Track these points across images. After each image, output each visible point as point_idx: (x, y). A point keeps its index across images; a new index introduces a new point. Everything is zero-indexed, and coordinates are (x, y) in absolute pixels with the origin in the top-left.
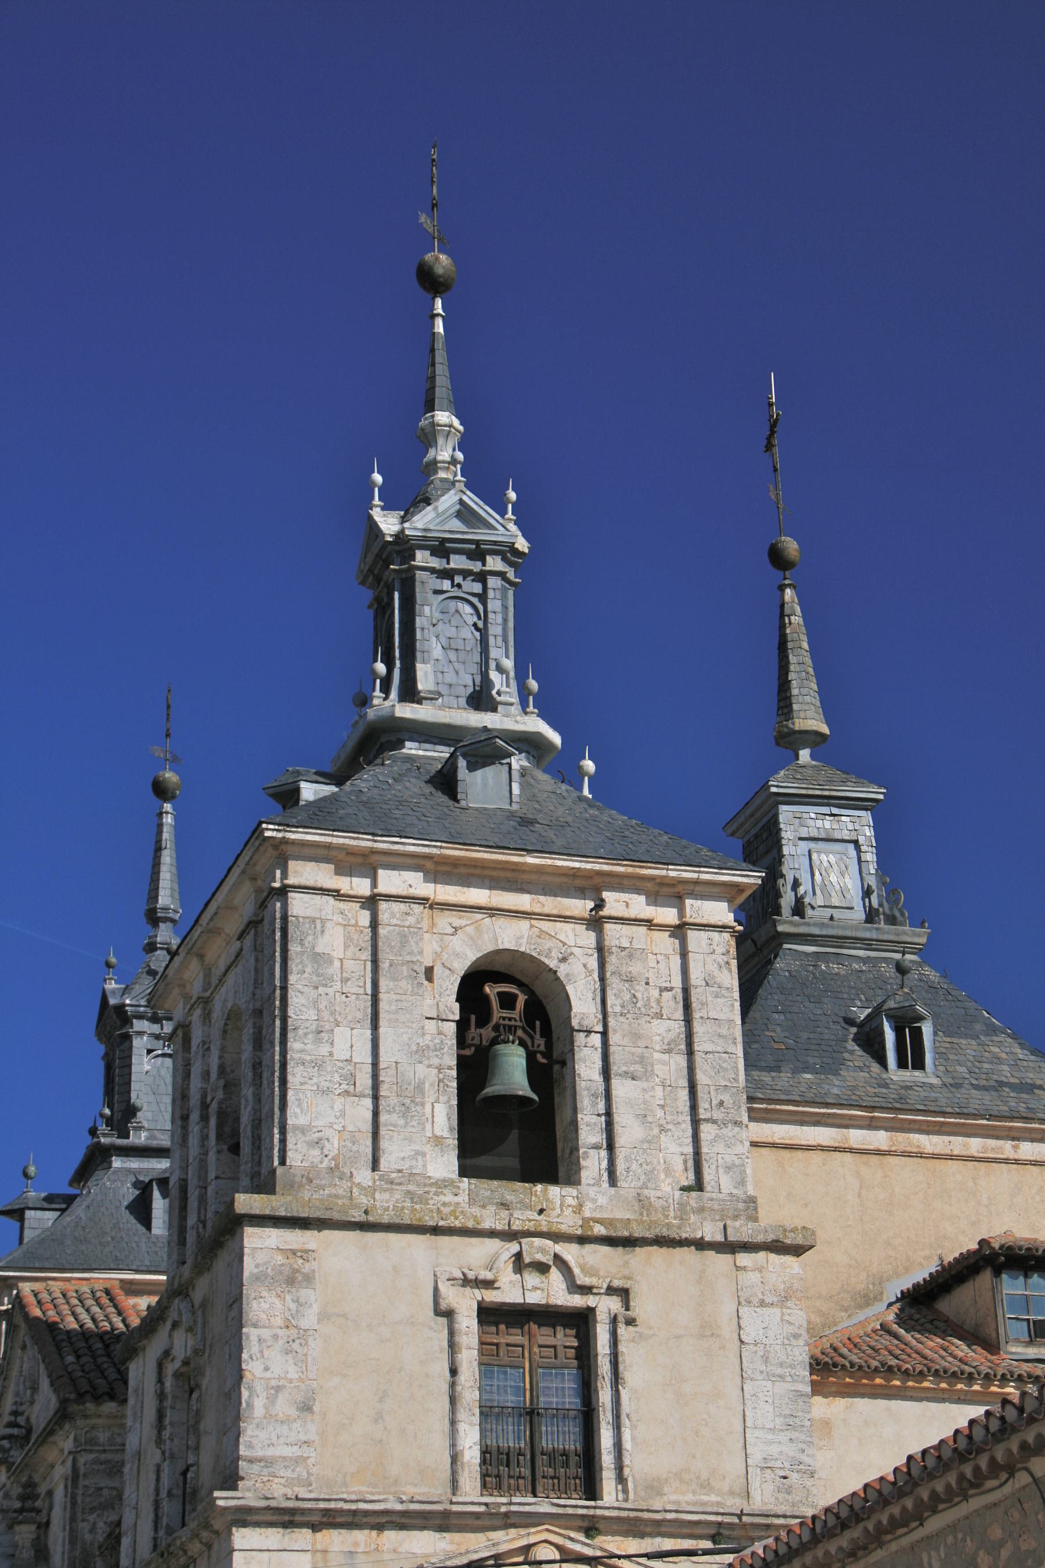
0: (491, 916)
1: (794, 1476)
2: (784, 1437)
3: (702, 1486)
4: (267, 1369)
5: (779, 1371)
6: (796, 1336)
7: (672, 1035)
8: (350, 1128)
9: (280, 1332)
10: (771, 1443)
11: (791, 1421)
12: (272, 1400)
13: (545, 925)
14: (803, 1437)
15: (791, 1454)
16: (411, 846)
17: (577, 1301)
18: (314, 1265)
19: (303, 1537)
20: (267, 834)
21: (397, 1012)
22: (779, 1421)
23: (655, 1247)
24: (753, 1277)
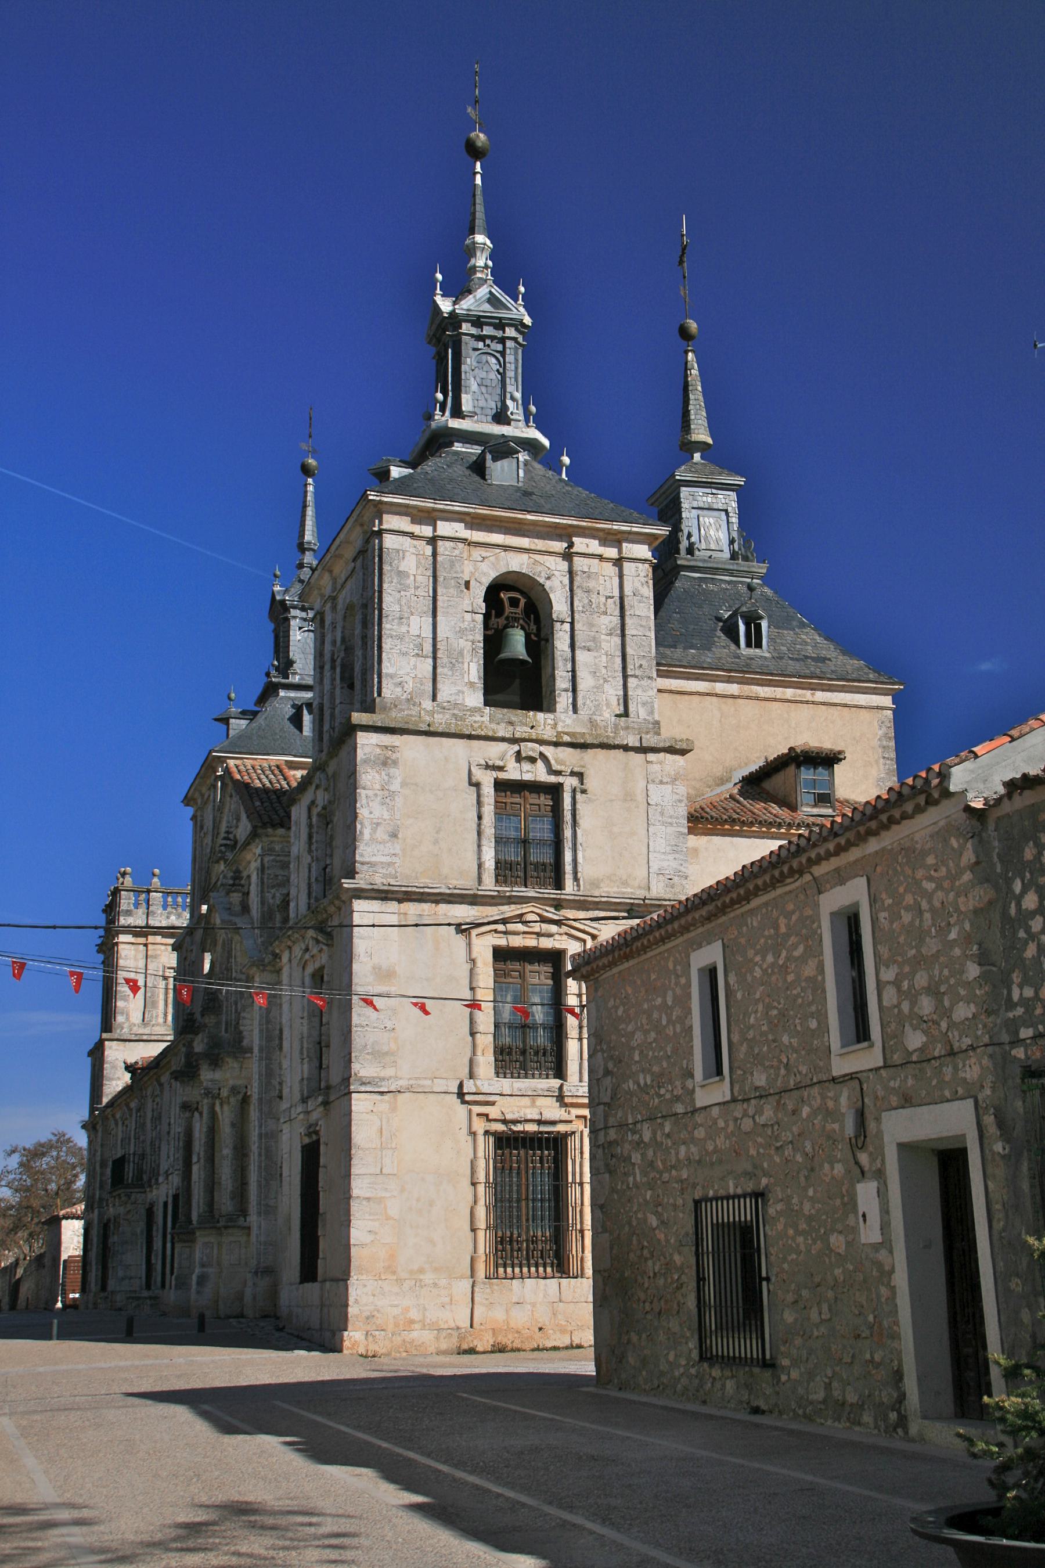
0: (505, 551)
2: (671, 857)
5: (670, 820)
7: (612, 625)
10: (664, 860)
11: (675, 848)
12: (374, 830)
13: (538, 557)
16: (457, 507)
17: (553, 779)
18: (398, 755)
21: (448, 607)
22: (668, 848)
24: (656, 767)
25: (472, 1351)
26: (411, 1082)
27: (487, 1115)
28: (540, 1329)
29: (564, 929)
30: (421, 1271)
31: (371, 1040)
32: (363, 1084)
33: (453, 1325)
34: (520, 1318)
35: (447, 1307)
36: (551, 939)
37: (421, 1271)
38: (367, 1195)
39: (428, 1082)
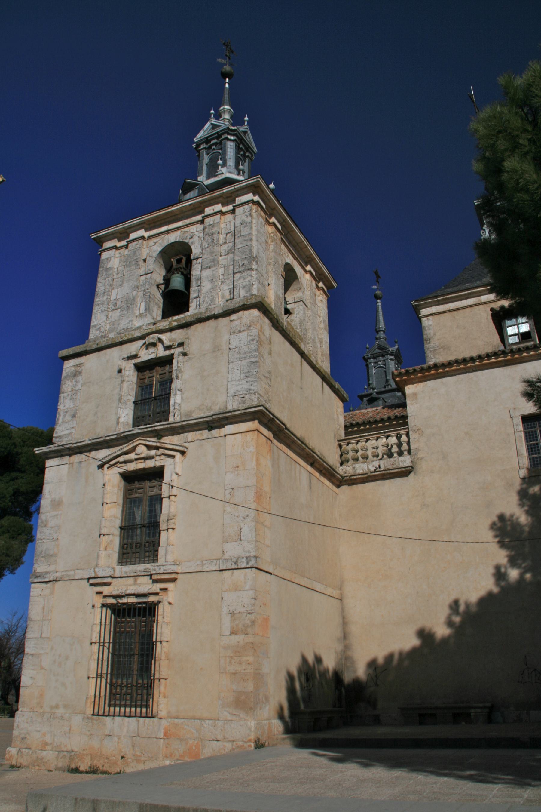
0: (168, 234)
1: (247, 396)
2: (244, 382)
3: (208, 410)
4: (64, 406)
5: (244, 356)
6: (253, 340)
8: (113, 321)
9: (69, 393)
10: (238, 385)
12: (65, 416)
13: (186, 229)
14: (252, 379)
15: (246, 387)
16: (135, 221)
17: (168, 353)
18: (83, 368)
19: (66, 459)
20: (93, 237)
23: (198, 324)
24: (236, 323)
25: (76, 770)
26: (63, 573)
27: (102, 593)
28: (122, 757)
29: (161, 451)
30: (57, 707)
31: (45, 548)
32: (37, 577)
33: (69, 749)
34: (110, 747)
35: (67, 735)
36: (153, 460)
37: (57, 707)
38: (32, 652)
39: (72, 573)
